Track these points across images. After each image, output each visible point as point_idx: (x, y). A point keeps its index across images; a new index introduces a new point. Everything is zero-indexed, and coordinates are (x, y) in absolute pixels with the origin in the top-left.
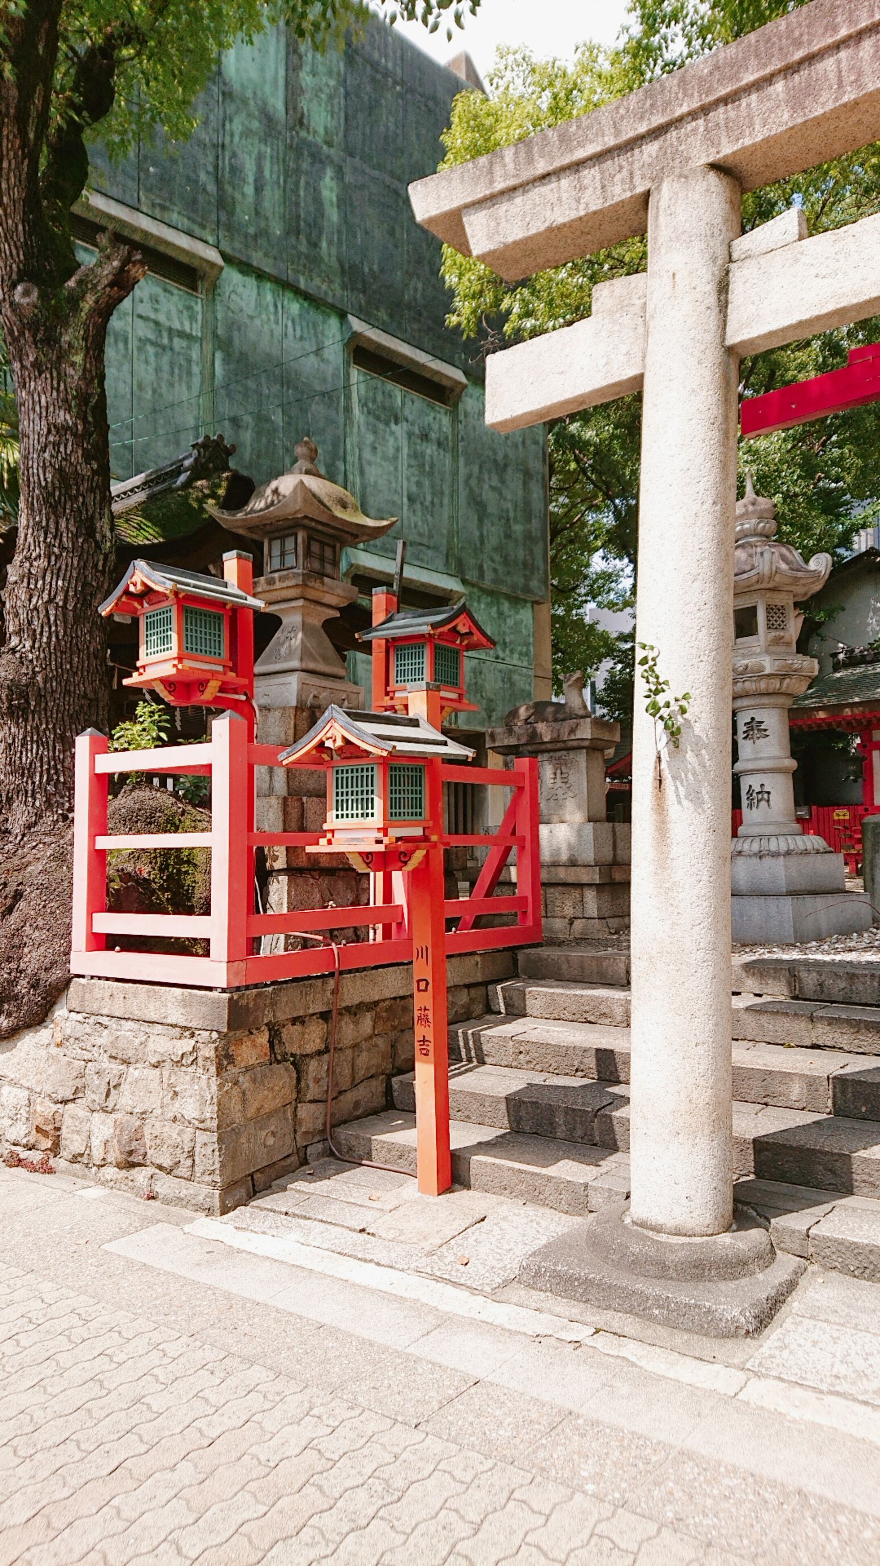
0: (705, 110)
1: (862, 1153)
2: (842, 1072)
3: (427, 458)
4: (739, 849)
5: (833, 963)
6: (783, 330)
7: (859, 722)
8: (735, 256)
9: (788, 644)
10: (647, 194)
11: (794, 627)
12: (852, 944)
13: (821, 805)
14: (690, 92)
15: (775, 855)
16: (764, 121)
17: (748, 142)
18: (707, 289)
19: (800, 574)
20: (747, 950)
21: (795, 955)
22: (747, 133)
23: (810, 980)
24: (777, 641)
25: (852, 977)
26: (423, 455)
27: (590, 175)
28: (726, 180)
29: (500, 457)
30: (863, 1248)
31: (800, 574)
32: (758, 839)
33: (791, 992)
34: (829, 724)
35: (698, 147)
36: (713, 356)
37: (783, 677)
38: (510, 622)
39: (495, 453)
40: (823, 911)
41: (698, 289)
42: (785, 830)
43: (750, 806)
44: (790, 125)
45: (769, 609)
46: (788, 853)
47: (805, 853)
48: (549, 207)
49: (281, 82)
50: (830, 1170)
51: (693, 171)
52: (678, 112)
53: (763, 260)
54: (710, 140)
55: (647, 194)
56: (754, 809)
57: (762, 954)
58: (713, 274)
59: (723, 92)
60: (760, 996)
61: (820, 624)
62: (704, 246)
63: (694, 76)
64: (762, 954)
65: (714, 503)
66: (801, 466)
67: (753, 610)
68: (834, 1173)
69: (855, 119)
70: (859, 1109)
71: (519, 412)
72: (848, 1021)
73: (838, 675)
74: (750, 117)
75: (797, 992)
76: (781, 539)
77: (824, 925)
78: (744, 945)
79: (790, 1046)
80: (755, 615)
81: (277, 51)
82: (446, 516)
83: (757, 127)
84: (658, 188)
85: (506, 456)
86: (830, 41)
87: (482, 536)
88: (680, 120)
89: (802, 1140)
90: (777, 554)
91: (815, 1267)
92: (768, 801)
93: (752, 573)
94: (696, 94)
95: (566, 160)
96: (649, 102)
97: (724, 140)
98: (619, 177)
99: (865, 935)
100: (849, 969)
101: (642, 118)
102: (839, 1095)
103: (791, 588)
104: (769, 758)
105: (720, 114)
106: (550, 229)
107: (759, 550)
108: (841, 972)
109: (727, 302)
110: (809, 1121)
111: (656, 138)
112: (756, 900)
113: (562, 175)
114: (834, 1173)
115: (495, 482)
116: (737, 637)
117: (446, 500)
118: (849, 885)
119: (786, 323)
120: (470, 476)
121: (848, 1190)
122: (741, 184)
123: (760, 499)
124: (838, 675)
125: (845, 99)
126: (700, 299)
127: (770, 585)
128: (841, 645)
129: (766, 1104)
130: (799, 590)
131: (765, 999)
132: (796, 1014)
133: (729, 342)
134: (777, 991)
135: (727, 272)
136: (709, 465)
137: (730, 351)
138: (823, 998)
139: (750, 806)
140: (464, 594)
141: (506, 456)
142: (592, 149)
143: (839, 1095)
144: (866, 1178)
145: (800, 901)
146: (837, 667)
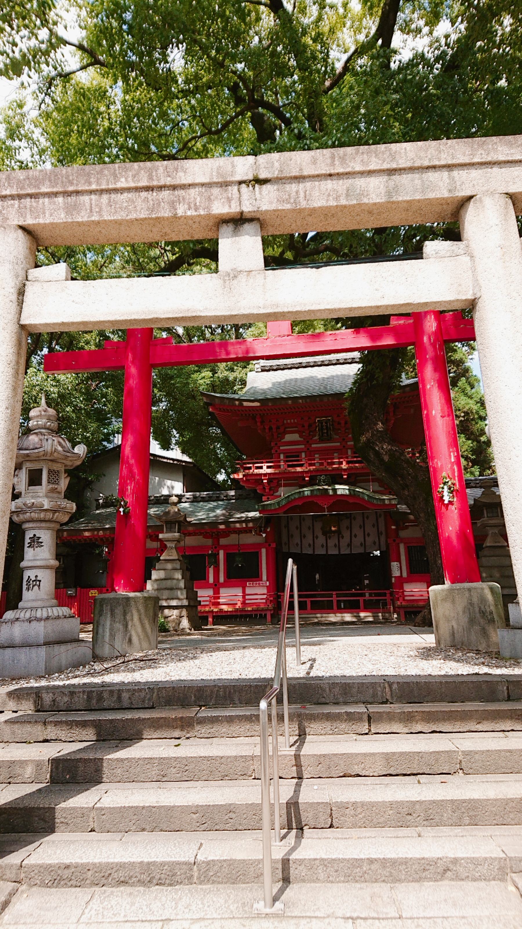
0: (20, 197)
1: (63, 805)
2: (58, 755)
4: (17, 617)
5: (64, 686)
6: (54, 324)
7: (107, 539)
9: (59, 493)
11: (64, 483)
12: (79, 673)
13: (81, 587)
14: (12, 185)
15: (39, 620)
16: (50, 214)
17: (41, 221)
19: (68, 454)
20: (14, 682)
21: (43, 683)
22: (41, 216)
23: (47, 698)
24: (53, 490)
25: (72, 693)
28: (28, 237)
30: (54, 866)
31: (68, 454)
32: (30, 610)
33: (35, 707)
34: (91, 540)
37: (55, 512)
40: (64, 654)
41: (6, 289)
42: (47, 604)
43: (28, 589)
44: (65, 220)
45: (50, 472)
46: (48, 618)
47: (58, 617)
50: (42, 819)
51: (10, 226)
53: (45, 285)
54: (21, 213)
56: (30, 591)
57: (23, 684)
58: (16, 284)
59: (30, 191)
60: (16, 712)
61: (91, 482)
63: (14, 178)
64: (23, 684)
65: (7, 408)
67: (40, 472)
68: (44, 820)
69: (98, 229)
70: (65, 777)
72: (66, 723)
73: (98, 512)
75: (39, 707)
76: (58, 431)
77: (64, 663)
78: (13, 679)
79: (30, 743)
80: (41, 474)
86: (87, 188)
89: (26, 803)
90: (56, 441)
91: (24, 887)
92: (39, 585)
94: (15, 187)
97: (28, 216)
99: (87, 667)
100: (72, 689)
102: (54, 770)
103: (64, 461)
104: (42, 560)
105: (27, 201)
107: (46, 437)
108: (66, 691)
110: (34, 790)
112: (24, 649)
114: (44, 820)
116: (29, 485)
118: (82, 636)
119: (55, 321)
121: (51, 829)
122: (37, 242)
123: (49, 409)
124: (98, 512)
125: (93, 218)
126: (7, 295)
127: (50, 458)
128: (101, 495)
129: (10, 783)
130: (69, 463)
131: (20, 713)
132: (36, 722)
134: (27, 708)
135: (24, 285)
136: (5, 386)
138: (55, 708)
139: (28, 589)
143: (54, 770)
144: (62, 820)
145: (51, 648)
146: (98, 507)
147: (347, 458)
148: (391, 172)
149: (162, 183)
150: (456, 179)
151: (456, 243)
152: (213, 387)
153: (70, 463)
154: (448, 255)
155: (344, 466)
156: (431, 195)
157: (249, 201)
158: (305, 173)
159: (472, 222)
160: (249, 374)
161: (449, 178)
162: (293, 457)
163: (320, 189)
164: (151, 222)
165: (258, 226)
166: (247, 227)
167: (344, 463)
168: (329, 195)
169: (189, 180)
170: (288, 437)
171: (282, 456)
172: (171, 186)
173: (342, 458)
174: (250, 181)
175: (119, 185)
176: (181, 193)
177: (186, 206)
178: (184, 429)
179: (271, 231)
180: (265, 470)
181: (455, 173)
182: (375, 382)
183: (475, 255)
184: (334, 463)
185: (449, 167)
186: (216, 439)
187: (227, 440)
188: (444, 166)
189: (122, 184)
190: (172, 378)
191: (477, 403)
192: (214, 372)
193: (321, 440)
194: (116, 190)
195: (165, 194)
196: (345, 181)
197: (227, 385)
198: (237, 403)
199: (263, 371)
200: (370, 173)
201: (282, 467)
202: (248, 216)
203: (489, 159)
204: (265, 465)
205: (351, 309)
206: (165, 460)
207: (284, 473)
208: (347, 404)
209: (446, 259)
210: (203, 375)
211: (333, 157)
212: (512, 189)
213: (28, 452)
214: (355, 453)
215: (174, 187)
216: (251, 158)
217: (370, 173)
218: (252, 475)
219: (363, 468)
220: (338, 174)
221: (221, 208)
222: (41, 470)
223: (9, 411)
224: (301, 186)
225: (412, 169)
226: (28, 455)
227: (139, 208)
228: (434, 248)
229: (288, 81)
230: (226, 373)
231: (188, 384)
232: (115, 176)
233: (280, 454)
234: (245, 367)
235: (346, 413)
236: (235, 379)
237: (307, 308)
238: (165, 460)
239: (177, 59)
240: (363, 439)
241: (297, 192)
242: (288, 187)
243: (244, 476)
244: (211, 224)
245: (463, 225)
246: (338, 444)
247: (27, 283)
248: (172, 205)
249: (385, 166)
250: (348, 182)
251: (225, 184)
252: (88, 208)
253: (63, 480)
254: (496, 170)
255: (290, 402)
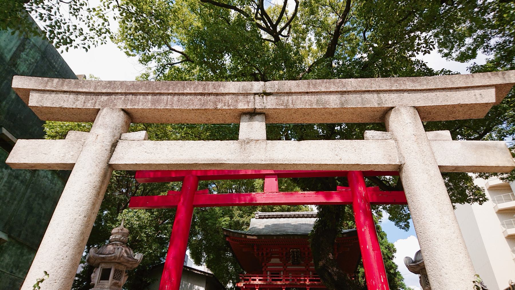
0: (126, 94)
3: (14, 185)
8: (122, 138)
10: (99, 109)
17: (136, 107)
18: (108, 144)
19: (130, 259)
26: (12, 183)
27: (82, 98)
29: (46, 194)
31: (130, 259)
35: (120, 103)
36: (103, 165)
38: (25, 258)
39: (45, 192)
45: (116, 271)
48: (63, 101)
49: (12, 52)
52: (117, 91)
53: (130, 142)
54: (124, 102)
55: (99, 109)
62: (111, 131)
65: (85, 217)
66: (154, 227)
67: (110, 270)
69: (169, 114)
71: (22, 162)
74: (139, 101)
81: (16, 43)
82: (12, 208)
83: (140, 105)
84: (102, 109)
85: (49, 194)
87: (26, 220)
88: (117, 93)
93: (113, 255)
95: (75, 90)
96: (109, 85)
98: (91, 101)
101: (105, 88)
103: (126, 264)
105: (130, 97)
106: (61, 108)
109: (114, 150)
111: (107, 95)
113: (72, 94)
115: (41, 202)
116: (101, 279)
117: (16, 202)
120: (31, 197)
123: (125, 229)
125: (167, 108)
127: (119, 261)
130: (129, 265)
133: (110, 163)
135: (118, 141)
137: (110, 167)
140: (7, 241)
141: (49, 194)
142: (84, 90)
147: (309, 277)
148: (343, 93)
149: (210, 92)
150: (382, 98)
151: (384, 132)
152: (230, 226)
153: (131, 266)
154: (380, 138)
155: (307, 283)
156: (368, 106)
157: (259, 103)
158: (293, 91)
159: (394, 121)
160: (252, 220)
161: (378, 97)
162: (275, 274)
163: (301, 100)
164: (202, 111)
165: (264, 117)
166: (257, 117)
167: (308, 280)
168: (306, 103)
169: (226, 91)
170: (274, 261)
171: (268, 273)
172: (215, 93)
173: (306, 277)
174: (261, 93)
175: (185, 91)
176: (221, 97)
177: (223, 104)
178: (210, 252)
179: (271, 121)
180: (257, 282)
181: (381, 95)
182: (327, 228)
183: (398, 139)
184: (301, 280)
185: (378, 92)
186: (228, 260)
187: (235, 261)
188: (374, 91)
189: (188, 91)
190: (207, 220)
191: (386, 248)
192: (231, 217)
193: (293, 264)
194: (183, 94)
195: (212, 97)
196: (316, 96)
197: (238, 225)
198: (243, 236)
199: (260, 218)
200: (331, 93)
201: (268, 280)
202: (259, 111)
203: (401, 88)
204: (257, 279)
205: (320, 165)
206: (196, 272)
207: (270, 285)
208: (310, 240)
209: (379, 141)
210: (225, 219)
211: (309, 84)
212: (417, 105)
213: (104, 256)
214: (314, 274)
215: (217, 94)
216: (262, 83)
217: (331, 93)
218: (250, 285)
219: (319, 285)
220: (312, 92)
221: (242, 105)
222: (110, 269)
223: (86, 219)
224: (290, 97)
225: (355, 92)
226: (103, 258)
227: (196, 103)
228: (371, 134)
229: (281, 72)
230: (238, 218)
231: (216, 224)
232: (184, 87)
233: (267, 271)
234: (250, 215)
235: (310, 246)
236: (243, 222)
237: (292, 162)
238: (196, 272)
239: (227, 60)
240: (321, 263)
241: (288, 100)
242: (282, 98)
243: (244, 285)
244: (237, 115)
245: (388, 123)
246: (304, 267)
247: (119, 140)
248: (215, 103)
249: (339, 90)
250: (318, 97)
251: (247, 94)
252: (165, 102)
253: (123, 277)
254: (406, 94)
255: (275, 238)
